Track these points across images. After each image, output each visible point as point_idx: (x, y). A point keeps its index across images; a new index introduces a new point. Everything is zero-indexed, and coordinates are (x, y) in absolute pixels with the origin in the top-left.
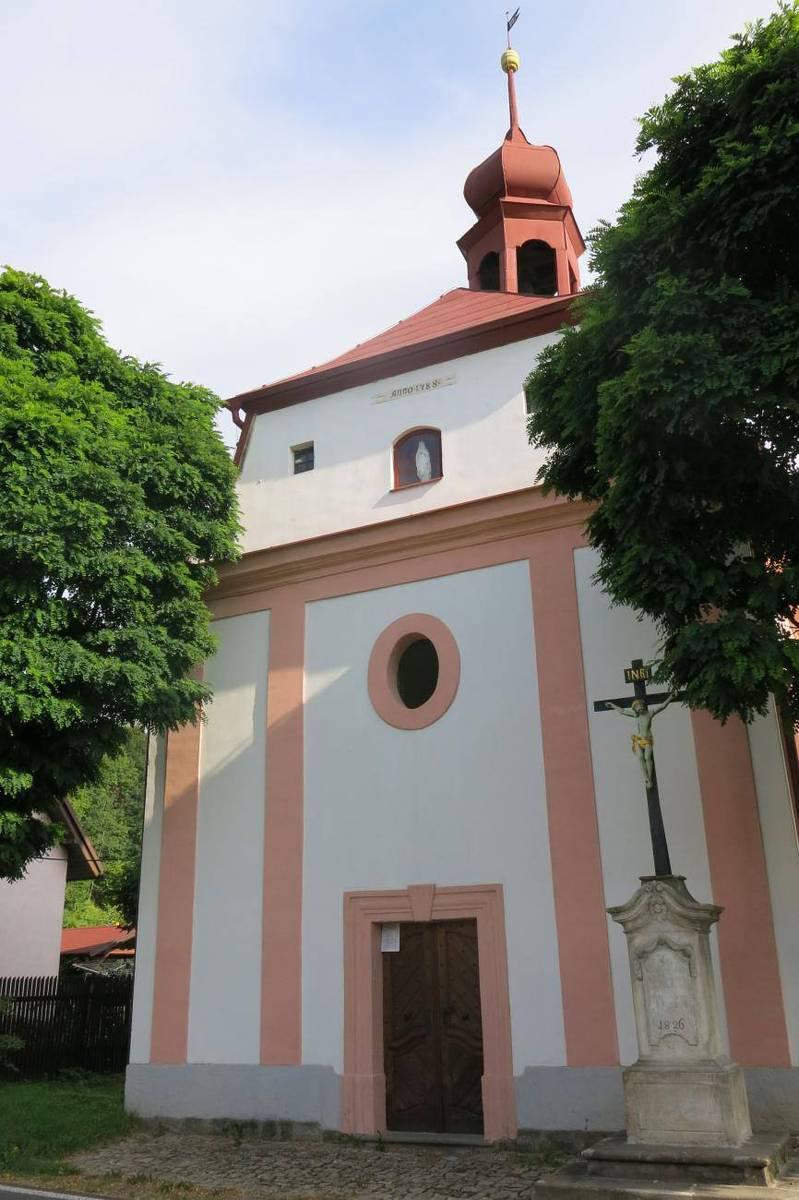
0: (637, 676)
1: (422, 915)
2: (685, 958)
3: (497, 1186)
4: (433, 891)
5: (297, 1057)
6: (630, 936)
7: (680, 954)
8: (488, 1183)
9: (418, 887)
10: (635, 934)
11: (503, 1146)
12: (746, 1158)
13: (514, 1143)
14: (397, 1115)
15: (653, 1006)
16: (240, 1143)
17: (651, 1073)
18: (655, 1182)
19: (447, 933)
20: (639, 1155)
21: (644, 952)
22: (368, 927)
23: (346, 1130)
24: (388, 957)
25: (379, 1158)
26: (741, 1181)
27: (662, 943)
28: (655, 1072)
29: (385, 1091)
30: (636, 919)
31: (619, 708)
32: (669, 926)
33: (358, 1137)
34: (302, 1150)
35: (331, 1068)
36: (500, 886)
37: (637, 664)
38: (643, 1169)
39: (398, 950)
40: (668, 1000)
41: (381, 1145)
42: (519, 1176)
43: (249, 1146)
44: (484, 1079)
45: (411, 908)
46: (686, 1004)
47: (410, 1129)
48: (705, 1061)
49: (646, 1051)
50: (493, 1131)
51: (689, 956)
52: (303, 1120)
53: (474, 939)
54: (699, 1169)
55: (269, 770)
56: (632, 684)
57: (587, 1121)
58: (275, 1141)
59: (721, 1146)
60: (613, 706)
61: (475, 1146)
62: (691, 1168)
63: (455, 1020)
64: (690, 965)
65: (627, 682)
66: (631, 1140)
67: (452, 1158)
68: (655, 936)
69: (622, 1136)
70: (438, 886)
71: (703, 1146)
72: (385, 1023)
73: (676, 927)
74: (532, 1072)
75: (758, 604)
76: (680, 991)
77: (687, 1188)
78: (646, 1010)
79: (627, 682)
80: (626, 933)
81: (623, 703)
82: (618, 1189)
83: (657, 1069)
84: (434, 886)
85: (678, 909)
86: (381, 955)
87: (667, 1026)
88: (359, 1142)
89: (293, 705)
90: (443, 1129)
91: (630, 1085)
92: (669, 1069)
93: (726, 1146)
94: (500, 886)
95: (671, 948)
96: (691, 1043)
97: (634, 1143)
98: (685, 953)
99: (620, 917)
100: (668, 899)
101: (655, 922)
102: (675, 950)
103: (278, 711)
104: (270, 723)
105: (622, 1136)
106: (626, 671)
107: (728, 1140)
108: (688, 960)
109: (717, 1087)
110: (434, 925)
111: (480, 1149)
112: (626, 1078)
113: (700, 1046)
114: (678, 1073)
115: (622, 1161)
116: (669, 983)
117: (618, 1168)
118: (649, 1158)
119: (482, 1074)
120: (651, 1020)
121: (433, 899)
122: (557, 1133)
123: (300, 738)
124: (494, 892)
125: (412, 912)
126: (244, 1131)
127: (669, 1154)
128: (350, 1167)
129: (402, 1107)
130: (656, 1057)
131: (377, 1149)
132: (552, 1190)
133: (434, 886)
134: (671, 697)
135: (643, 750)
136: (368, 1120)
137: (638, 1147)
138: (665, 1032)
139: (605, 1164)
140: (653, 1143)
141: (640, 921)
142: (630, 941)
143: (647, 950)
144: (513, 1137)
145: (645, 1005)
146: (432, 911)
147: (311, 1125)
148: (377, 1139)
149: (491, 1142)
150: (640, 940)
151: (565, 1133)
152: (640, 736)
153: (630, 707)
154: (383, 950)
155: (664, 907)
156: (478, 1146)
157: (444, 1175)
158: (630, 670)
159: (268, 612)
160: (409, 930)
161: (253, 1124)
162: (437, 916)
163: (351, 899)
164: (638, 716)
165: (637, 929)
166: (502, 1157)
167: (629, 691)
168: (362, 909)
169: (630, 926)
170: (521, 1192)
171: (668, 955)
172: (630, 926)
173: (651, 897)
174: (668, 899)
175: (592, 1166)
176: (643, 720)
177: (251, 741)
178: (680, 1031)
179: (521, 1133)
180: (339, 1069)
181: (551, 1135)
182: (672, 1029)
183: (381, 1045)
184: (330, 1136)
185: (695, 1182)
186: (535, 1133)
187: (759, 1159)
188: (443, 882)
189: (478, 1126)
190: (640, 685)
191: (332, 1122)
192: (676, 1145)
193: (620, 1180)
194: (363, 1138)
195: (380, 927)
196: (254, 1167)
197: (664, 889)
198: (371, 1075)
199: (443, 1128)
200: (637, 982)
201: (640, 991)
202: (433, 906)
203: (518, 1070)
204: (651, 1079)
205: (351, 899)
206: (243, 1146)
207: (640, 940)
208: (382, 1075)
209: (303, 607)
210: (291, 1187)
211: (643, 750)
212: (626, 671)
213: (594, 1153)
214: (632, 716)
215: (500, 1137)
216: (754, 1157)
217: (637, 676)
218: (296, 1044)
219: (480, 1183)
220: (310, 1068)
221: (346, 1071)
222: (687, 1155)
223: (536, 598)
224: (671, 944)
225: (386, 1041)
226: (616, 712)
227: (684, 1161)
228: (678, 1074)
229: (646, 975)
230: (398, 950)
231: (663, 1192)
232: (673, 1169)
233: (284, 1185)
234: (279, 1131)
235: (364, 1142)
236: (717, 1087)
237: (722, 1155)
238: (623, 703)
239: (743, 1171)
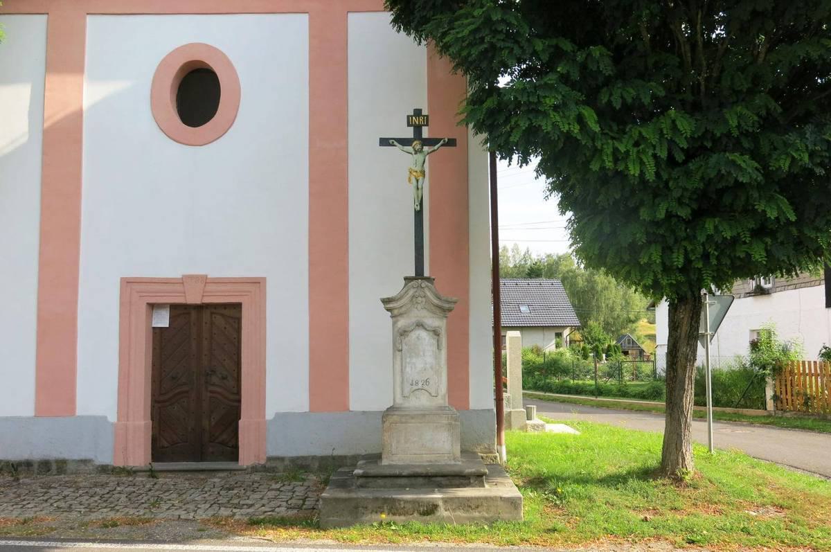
0: (417, 123)
1: (194, 298)
2: (435, 337)
3: (265, 498)
4: (205, 280)
5: (72, 410)
6: (394, 319)
7: (431, 333)
8: (257, 496)
9: (191, 277)
10: (399, 318)
11: (255, 469)
12: (473, 470)
13: (264, 466)
14: (159, 451)
15: (408, 369)
16: (18, 479)
17: (403, 416)
18: (408, 489)
19: (212, 313)
20: (392, 472)
21: (405, 331)
22: (144, 308)
23: (121, 464)
24: (158, 332)
25: (155, 484)
26: (468, 485)
27: (420, 325)
28: (407, 415)
29: (151, 434)
30: (401, 307)
31: (401, 146)
32: (425, 313)
33: (129, 468)
34: (82, 482)
35: (106, 417)
36: (264, 279)
37: (418, 113)
38: (400, 481)
39: (168, 326)
40: (420, 366)
41: (152, 474)
42: (278, 490)
43: (27, 480)
44: (241, 422)
45: (184, 293)
46: (432, 368)
47: (172, 460)
48: (441, 407)
49: (399, 401)
50: (247, 457)
51: (438, 335)
52: (76, 457)
53: (239, 320)
54: (439, 479)
55: (45, 165)
56: (412, 129)
57: (334, 449)
58: (51, 475)
59: (449, 463)
60: (396, 143)
61: (230, 470)
62: (433, 479)
63: (215, 379)
64: (438, 341)
65: (409, 125)
66: (385, 462)
67: (216, 480)
68: (414, 320)
69: (377, 458)
70: (209, 277)
71: (437, 463)
72: (153, 381)
73: (431, 314)
74: (279, 416)
75: (565, 72)
76: (429, 359)
77: (433, 492)
78: (402, 371)
79: (409, 125)
80: (392, 317)
81: (404, 142)
82: (387, 496)
83: (407, 413)
84: (207, 276)
85: (436, 301)
86: (152, 330)
87: (417, 383)
88: (131, 472)
89: (72, 108)
90: (202, 459)
91: (387, 424)
92: (416, 413)
93: (453, 462)
94: (264, 279)
95: (426, 329)
96: (433, 394)
97: (386, 464)
98: (436, 333)
99: (391, 305)
100: (428, 294)
101: (415, 310)
102: (428, 330)
103: (56, 113)
104: (45, 125)
105: (377, 458)
106: (408, 117)
107: (454, 459)
108: (437, 337)
109: (450, 424)
110: (201, 308)
111: (236, 473)
112: (384, 420)
113: (439, 397)
114: (424, 415)
115: (238, 470)
116: (421, 353)
117: (380, 481)
118: (404, 474)
119: (240, 419)
120: (405, 380)
121: (205, 286)
122: (298, 458)
123: (79, 141)
124: (259, 283)
125: (185, 296)
126: (19, 469)
127: (419, 470)
128: (134, 492)
129: (166, 444)
130: (406, 405)
131: (149, 476)
132: (337, 500)
133: (207, 276)
134: (442, 142)
135: (417, 181)
136: (139, 456)
137: (390, 466)
138: (415, 387)
139: (370, 480)
140: (401, 463)
141: (403, 309)
142: (394, 323)
143: (407, 329)
144: (263, 462)
145: (402, 369)
146: (203, 296)
147: (85, 462)
148: (148, 469)
149: (245, 467)
150: (402, 323)
151: (303, 458)
152: (416, 169)
153: (411, 145)
154: (154, 325)
155: (424, 299)
156: (235, 470)
157: (219, 493)
158: (412, 116)
159: (45, 17)
160: (178, 311)
161: (28, 464)
162: (207, 300)
163: (127, 283)
164: (416, 153)
165: (401, 315)
166: (256, 477)
167: (409, 133)
168: (138, 292)
169: (396, 312)
170: (287, 501)
171: (423, 334)
172: (396, 312)
173: (416, 292)
174: (428, 294)
175: (361, 481)
176: (420, 157)
177: (25, 139)
178: (425, 387)
179: (270, 459)
180: (112, 418)
181: (294, 460)
182: (420, 386)
183: (150, 398)
184: (104, 469)
185: (437, 488)
186: (282, 459)
187: (482, 470)
188: (213, 274)
189: (234, 456)
190: (418, 130)
191: (105, 457)
192: (418, 464)
193: (382, 489)
194: (134, 469)
195: (152, 307)
196: (45, 498)
197: (427, 286)
198: (141, 423)
199: (201, 457)
200: (397, 353)
201: (398, 358)
202: (204, 292)
203: (270, 415)
204: (403, 420)
205: (127, 283)
206: (21, 481)
207: (402, 323)
208: (150, 422)
209: (85, 19)
210: (90, 511)
211: (417, 181)
212: (408, 117)
213: (363, 473)
214: (411, 153)
215: (252, 463)
216: (479, 468)
217: (417, 123)
218: (72, 401)
219: (251, 497)
220: (82, 417)
221: (119, 419)
222: (431, 470)
223: (312, 49)
224: (426, 327)
225: (153, 395)
226: (398, 149)
227: (430, 474)
228: (423, 416)
229: (405, 348)
230: (168, 326)
231: (422, 496)
232: (420, 480)
233: (83, 510)
234: (54, 467)
235: (135, 472)
236: (450, 424)
237: (456, 469)
238: (404, 142)
239: (470, 478)
